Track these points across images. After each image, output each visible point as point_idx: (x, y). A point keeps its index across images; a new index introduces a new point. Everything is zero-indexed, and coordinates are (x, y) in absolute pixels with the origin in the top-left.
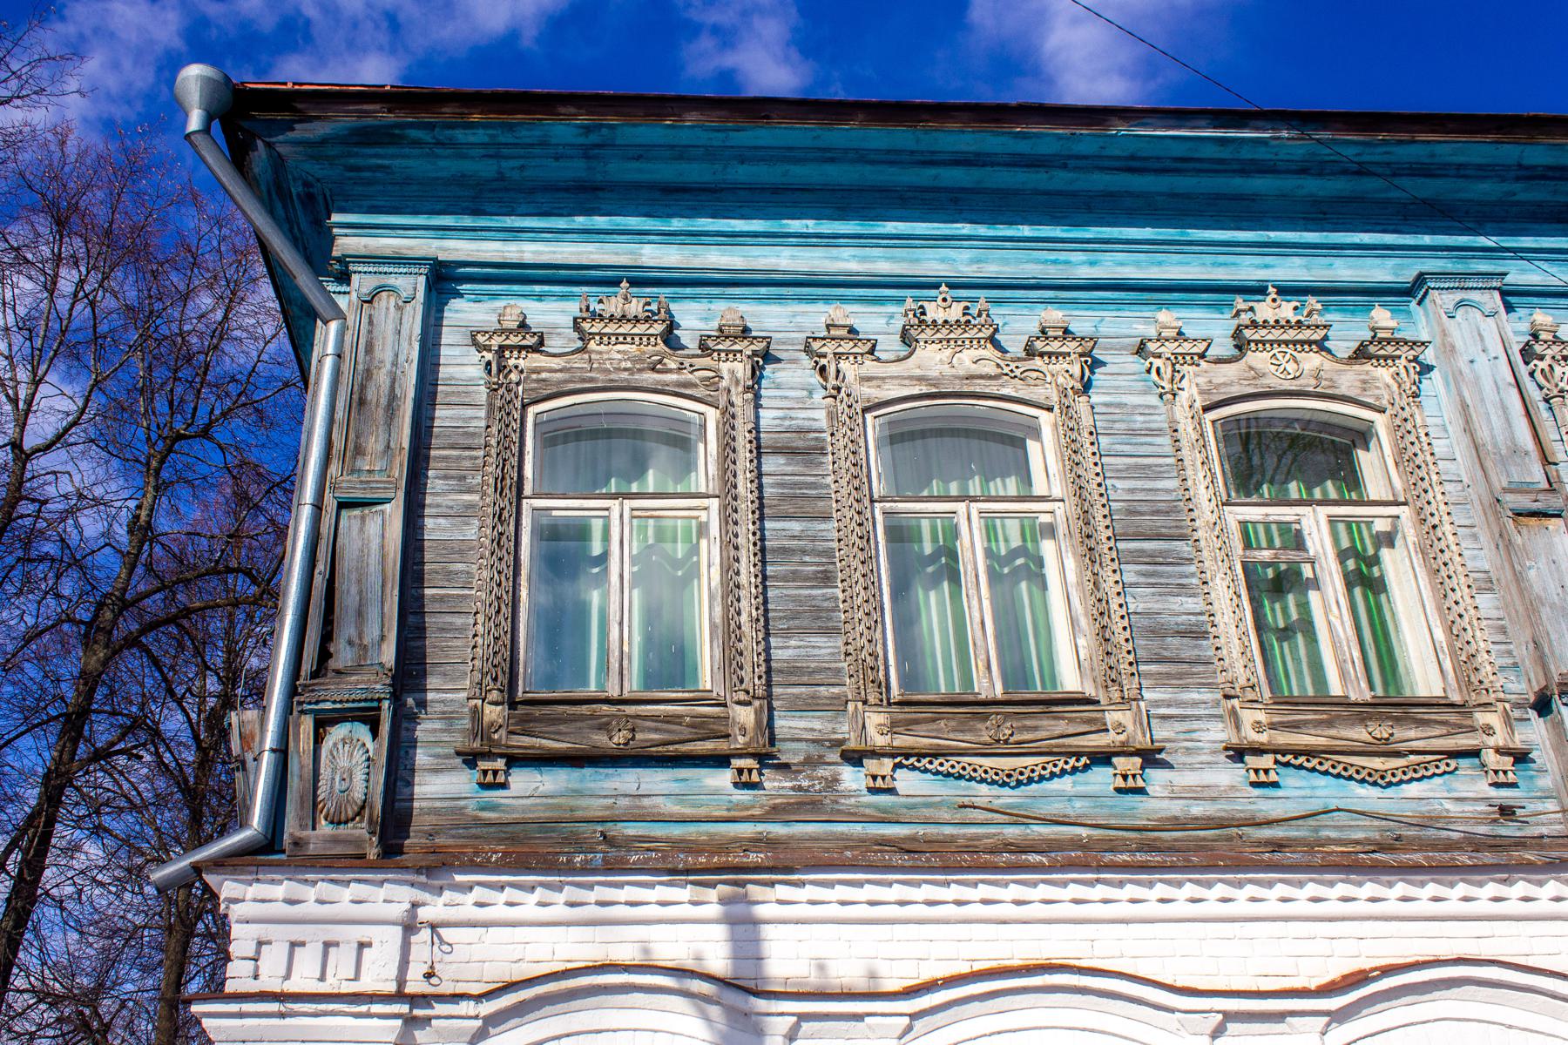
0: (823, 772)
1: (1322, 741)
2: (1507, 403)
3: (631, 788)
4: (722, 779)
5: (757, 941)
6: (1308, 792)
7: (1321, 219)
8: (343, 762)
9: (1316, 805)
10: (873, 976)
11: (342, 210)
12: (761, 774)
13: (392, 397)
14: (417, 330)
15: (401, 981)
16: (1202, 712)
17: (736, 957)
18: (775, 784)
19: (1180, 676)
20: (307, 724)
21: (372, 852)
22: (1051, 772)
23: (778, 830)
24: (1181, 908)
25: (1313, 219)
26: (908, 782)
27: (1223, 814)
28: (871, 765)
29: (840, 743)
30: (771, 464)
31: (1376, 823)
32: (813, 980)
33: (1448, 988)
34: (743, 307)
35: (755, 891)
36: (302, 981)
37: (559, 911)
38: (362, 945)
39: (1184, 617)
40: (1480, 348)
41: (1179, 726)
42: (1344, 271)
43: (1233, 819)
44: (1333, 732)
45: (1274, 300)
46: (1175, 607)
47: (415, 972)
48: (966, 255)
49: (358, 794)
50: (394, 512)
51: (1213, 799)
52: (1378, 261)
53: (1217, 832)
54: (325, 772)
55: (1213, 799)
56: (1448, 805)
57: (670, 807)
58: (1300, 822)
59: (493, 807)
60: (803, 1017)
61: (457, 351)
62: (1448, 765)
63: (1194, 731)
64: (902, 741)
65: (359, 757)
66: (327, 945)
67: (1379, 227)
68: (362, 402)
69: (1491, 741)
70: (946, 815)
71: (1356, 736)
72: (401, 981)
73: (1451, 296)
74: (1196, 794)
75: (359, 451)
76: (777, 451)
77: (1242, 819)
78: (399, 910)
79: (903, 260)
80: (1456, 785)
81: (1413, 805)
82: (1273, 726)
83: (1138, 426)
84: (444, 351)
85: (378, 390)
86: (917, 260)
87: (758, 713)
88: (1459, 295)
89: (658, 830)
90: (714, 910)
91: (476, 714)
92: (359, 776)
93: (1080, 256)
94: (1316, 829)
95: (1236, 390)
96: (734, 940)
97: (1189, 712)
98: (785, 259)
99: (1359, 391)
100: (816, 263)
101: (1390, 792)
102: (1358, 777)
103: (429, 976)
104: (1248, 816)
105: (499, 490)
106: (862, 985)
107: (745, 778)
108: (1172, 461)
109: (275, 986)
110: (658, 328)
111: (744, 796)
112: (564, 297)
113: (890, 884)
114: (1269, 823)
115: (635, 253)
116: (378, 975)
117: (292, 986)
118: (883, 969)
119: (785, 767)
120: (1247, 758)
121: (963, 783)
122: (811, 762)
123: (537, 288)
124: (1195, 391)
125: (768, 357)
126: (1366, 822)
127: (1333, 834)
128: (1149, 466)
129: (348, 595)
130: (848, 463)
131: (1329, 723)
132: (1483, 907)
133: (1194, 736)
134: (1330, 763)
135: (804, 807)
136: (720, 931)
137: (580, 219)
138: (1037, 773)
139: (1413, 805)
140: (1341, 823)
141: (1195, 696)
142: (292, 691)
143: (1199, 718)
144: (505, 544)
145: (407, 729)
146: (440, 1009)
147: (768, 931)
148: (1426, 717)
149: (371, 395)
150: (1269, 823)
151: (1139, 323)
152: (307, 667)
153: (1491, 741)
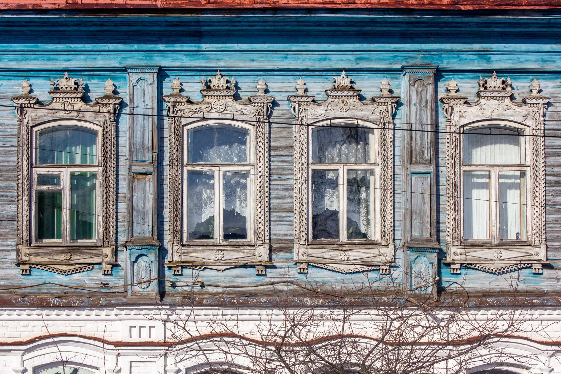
1: (47, 260)
2: (146, 125)
6: (40, 277)
7: (94, 38)
9: (42, 281)
12: (265, 271)
16: (10, 249)
22: (515, 269)
25: (91, 38)
27: (10, 284)
31: (61, 287)
33: (64, 342)
39: (10, 213)
40: (142, 100)
43: (13, 286)
44: (51, 257)
45: (66, 78)
46: (8, 209)
51: (8, 279)
52: (115, 56)
53: (7, 290)
55: (8, 279)
56: (87, 281)
58: (35, 287)
62: (89, 268)
63: (6, 255)
67: (118, 41)
69: (106, 260)
71: (58, 259)
73: (137, 76)
77: (16, 286)
80: (91, 274)
81: (75, 281)
83: (8, 133)
88: (139, 76)
94: (40, 290)
95: (46, 119)
97: (5, 248)
99: (93, 119)
101: (68, 277)
102: (82, 271)
104: (19, 285)
107: (24, 273)
108: (16, 149)
113: (202, 309)
114: (25, 287)
120: (452, 266)
121: (488, 274)
124: (30, 119)
126: (58, 287)
127: (45, 291)
128: (9, 151)
130: (175, 140)
131: (50, 254)
132: (83, 317)
133: (6, 257)
134: (48, 267)
138: (513, 268)
139: (75, 281)
140: (49, 288)
141: (9, 243)
143: (8, 251)
148: (85, 251)
151: (16, 86)
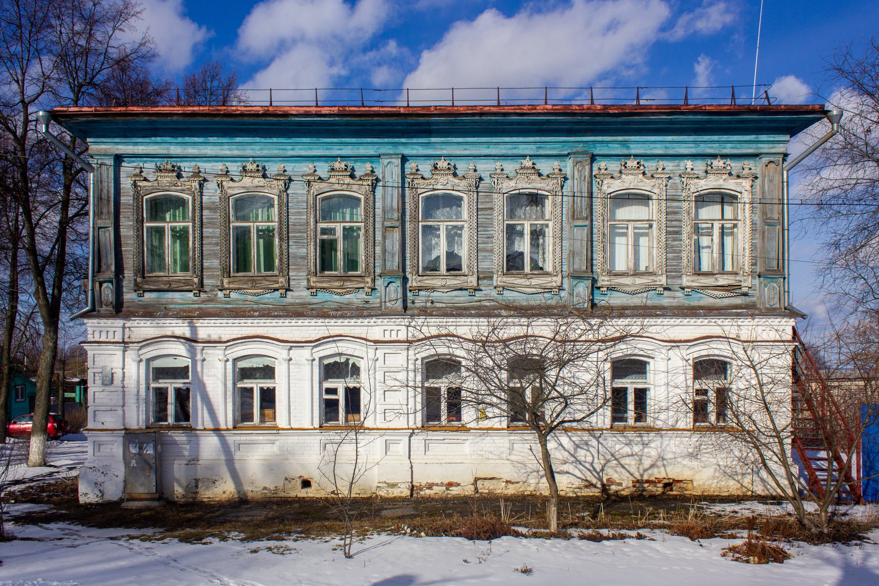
0: (214, 293)
3: (171, 297)
4: (191, 295)
5: (196, 331)
8: (106, 293)
9: (324, 300)
10: (220, 338)
11: (90, 137)
13: (109, 197)
14: (113, 176)
15: (123, 339)
17: (192, 334)
18: (203, 295)
19: (299, 269)
20: (97, 284)
21: (114, 313)
23: (203, 306)
24: (286, 324)
26: (233, 295)
28: (224, 292)
29: (218, 286)
30: (205, 212)
32: (208, 339)
34: (199, 164)
35: (195, 321)
36: (103, 339)
37: (154, 325)
38: (115, 332)
41: (297, 281)
42: (362, 151)
47: (126, 336)
48: (258, 148)
49: (110, 300)
50: (111, 229)
54: (103, 295)
57: (180, 301)
59: (141, 301)
60: (204, 347)
61: (124, 179)
64: (231, 286)
65: (110, 291)
66: (107, 332)
68: (101, 199)
69: (367, 285)
70: (240, 303)
72: (123, 339)
74: (297, 297)
75: (102, 213)
76: (207, 209)
78: (121, 325)
79: (241, 150)
82: (317, 282)
84: (121, 179)
85: (104, 196)
86: (245, 150)
87: (199, 280)
88: (389, 160)
89: (177, 306)
90: (186, 324)
91: (135, 280)
92: (110, 296)
93: (290, 147)
95: (326, 190)
96: (191, 330)
98: (209, 150)
100: (218, 151)
103: (129, 337)
105: (137, 222)
106: (218, 340)
109: (98, 340)
110: (175, 174)
111: (196, 298)
112: (151, 161)
114: (313, 304)
115: (98, 270)
116: (118, 338)
117: (101, 340)
118: (223, 336)
119: (205, 292)
122: (211, 291)
123: (144, 159)
125: (205, 180)
129: (103, 253)
131: (330, 282)
135: (210, 300)
136: (188, 329)
137: (153, 138)
142: (93, 276)
144: (140, 237)
145: (174, 216)
146: (130, 345)
147: (199, 328)
149: (103, 197)
150: (313, 304)
152: (96, 271)
153: (367, 285)
